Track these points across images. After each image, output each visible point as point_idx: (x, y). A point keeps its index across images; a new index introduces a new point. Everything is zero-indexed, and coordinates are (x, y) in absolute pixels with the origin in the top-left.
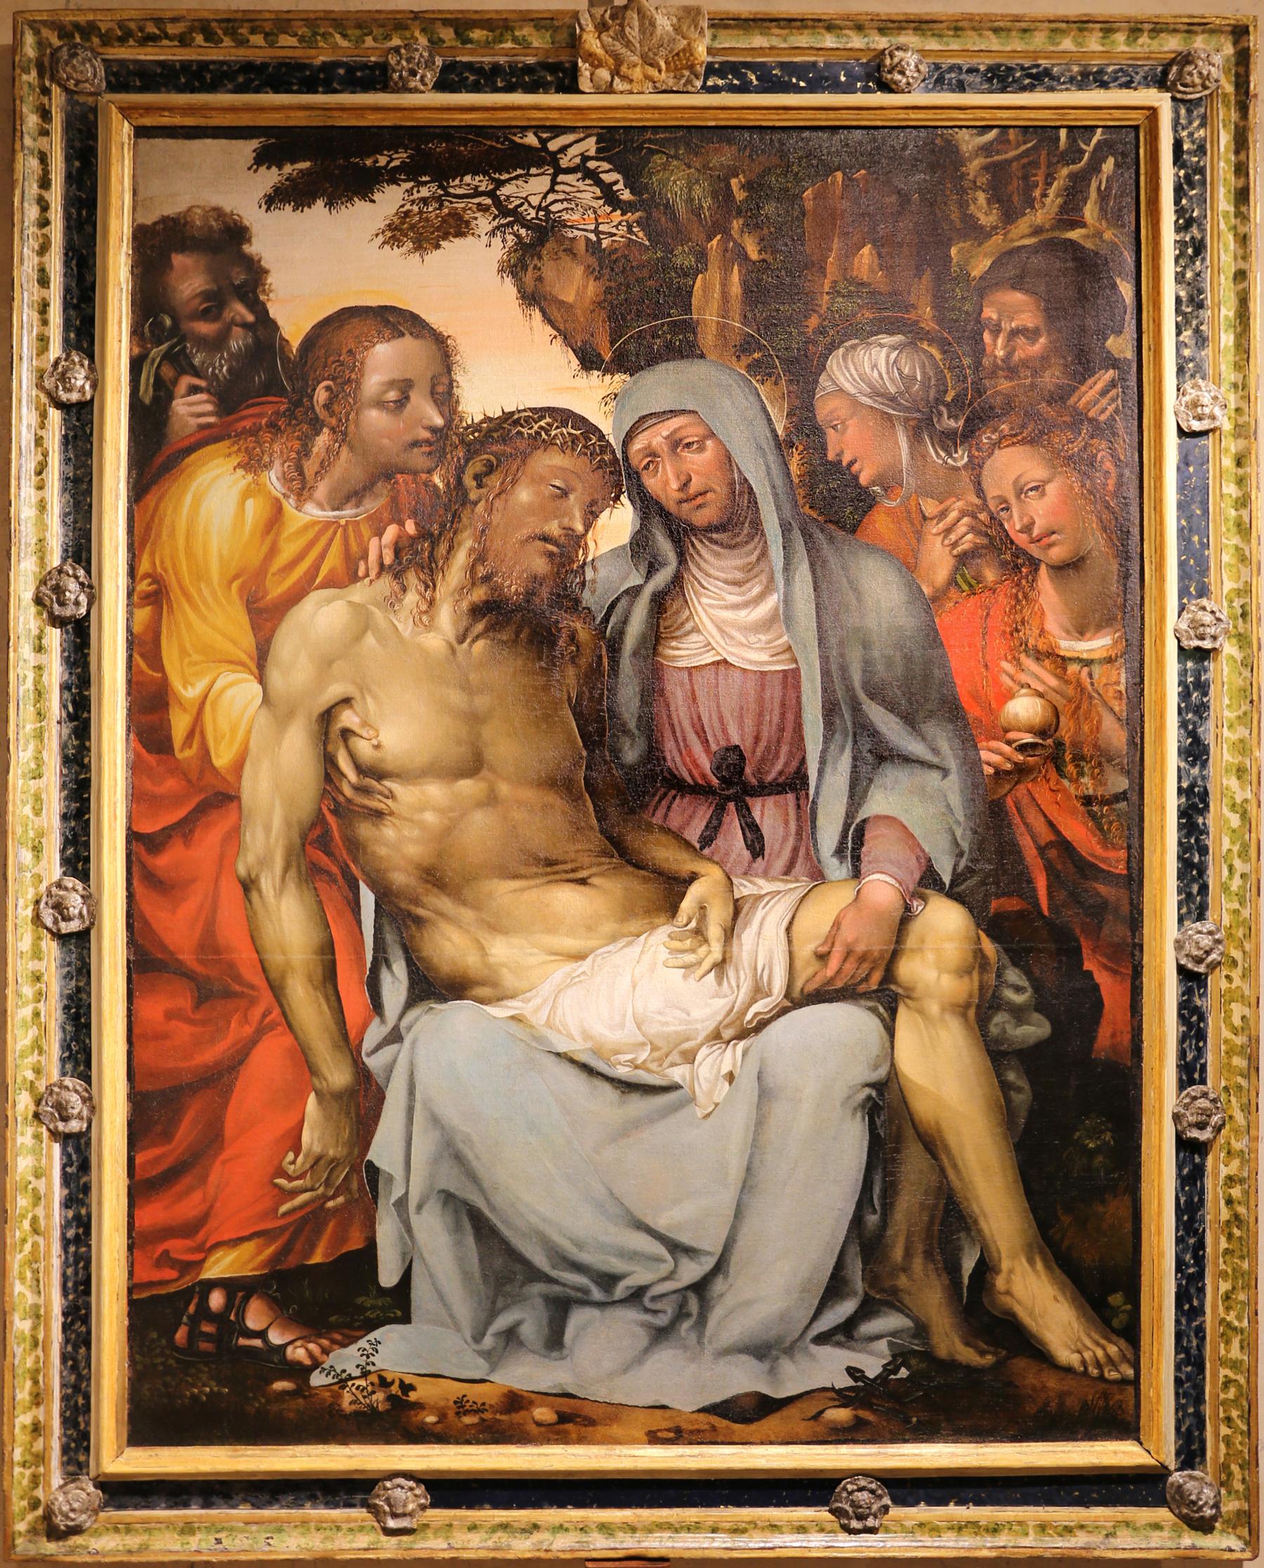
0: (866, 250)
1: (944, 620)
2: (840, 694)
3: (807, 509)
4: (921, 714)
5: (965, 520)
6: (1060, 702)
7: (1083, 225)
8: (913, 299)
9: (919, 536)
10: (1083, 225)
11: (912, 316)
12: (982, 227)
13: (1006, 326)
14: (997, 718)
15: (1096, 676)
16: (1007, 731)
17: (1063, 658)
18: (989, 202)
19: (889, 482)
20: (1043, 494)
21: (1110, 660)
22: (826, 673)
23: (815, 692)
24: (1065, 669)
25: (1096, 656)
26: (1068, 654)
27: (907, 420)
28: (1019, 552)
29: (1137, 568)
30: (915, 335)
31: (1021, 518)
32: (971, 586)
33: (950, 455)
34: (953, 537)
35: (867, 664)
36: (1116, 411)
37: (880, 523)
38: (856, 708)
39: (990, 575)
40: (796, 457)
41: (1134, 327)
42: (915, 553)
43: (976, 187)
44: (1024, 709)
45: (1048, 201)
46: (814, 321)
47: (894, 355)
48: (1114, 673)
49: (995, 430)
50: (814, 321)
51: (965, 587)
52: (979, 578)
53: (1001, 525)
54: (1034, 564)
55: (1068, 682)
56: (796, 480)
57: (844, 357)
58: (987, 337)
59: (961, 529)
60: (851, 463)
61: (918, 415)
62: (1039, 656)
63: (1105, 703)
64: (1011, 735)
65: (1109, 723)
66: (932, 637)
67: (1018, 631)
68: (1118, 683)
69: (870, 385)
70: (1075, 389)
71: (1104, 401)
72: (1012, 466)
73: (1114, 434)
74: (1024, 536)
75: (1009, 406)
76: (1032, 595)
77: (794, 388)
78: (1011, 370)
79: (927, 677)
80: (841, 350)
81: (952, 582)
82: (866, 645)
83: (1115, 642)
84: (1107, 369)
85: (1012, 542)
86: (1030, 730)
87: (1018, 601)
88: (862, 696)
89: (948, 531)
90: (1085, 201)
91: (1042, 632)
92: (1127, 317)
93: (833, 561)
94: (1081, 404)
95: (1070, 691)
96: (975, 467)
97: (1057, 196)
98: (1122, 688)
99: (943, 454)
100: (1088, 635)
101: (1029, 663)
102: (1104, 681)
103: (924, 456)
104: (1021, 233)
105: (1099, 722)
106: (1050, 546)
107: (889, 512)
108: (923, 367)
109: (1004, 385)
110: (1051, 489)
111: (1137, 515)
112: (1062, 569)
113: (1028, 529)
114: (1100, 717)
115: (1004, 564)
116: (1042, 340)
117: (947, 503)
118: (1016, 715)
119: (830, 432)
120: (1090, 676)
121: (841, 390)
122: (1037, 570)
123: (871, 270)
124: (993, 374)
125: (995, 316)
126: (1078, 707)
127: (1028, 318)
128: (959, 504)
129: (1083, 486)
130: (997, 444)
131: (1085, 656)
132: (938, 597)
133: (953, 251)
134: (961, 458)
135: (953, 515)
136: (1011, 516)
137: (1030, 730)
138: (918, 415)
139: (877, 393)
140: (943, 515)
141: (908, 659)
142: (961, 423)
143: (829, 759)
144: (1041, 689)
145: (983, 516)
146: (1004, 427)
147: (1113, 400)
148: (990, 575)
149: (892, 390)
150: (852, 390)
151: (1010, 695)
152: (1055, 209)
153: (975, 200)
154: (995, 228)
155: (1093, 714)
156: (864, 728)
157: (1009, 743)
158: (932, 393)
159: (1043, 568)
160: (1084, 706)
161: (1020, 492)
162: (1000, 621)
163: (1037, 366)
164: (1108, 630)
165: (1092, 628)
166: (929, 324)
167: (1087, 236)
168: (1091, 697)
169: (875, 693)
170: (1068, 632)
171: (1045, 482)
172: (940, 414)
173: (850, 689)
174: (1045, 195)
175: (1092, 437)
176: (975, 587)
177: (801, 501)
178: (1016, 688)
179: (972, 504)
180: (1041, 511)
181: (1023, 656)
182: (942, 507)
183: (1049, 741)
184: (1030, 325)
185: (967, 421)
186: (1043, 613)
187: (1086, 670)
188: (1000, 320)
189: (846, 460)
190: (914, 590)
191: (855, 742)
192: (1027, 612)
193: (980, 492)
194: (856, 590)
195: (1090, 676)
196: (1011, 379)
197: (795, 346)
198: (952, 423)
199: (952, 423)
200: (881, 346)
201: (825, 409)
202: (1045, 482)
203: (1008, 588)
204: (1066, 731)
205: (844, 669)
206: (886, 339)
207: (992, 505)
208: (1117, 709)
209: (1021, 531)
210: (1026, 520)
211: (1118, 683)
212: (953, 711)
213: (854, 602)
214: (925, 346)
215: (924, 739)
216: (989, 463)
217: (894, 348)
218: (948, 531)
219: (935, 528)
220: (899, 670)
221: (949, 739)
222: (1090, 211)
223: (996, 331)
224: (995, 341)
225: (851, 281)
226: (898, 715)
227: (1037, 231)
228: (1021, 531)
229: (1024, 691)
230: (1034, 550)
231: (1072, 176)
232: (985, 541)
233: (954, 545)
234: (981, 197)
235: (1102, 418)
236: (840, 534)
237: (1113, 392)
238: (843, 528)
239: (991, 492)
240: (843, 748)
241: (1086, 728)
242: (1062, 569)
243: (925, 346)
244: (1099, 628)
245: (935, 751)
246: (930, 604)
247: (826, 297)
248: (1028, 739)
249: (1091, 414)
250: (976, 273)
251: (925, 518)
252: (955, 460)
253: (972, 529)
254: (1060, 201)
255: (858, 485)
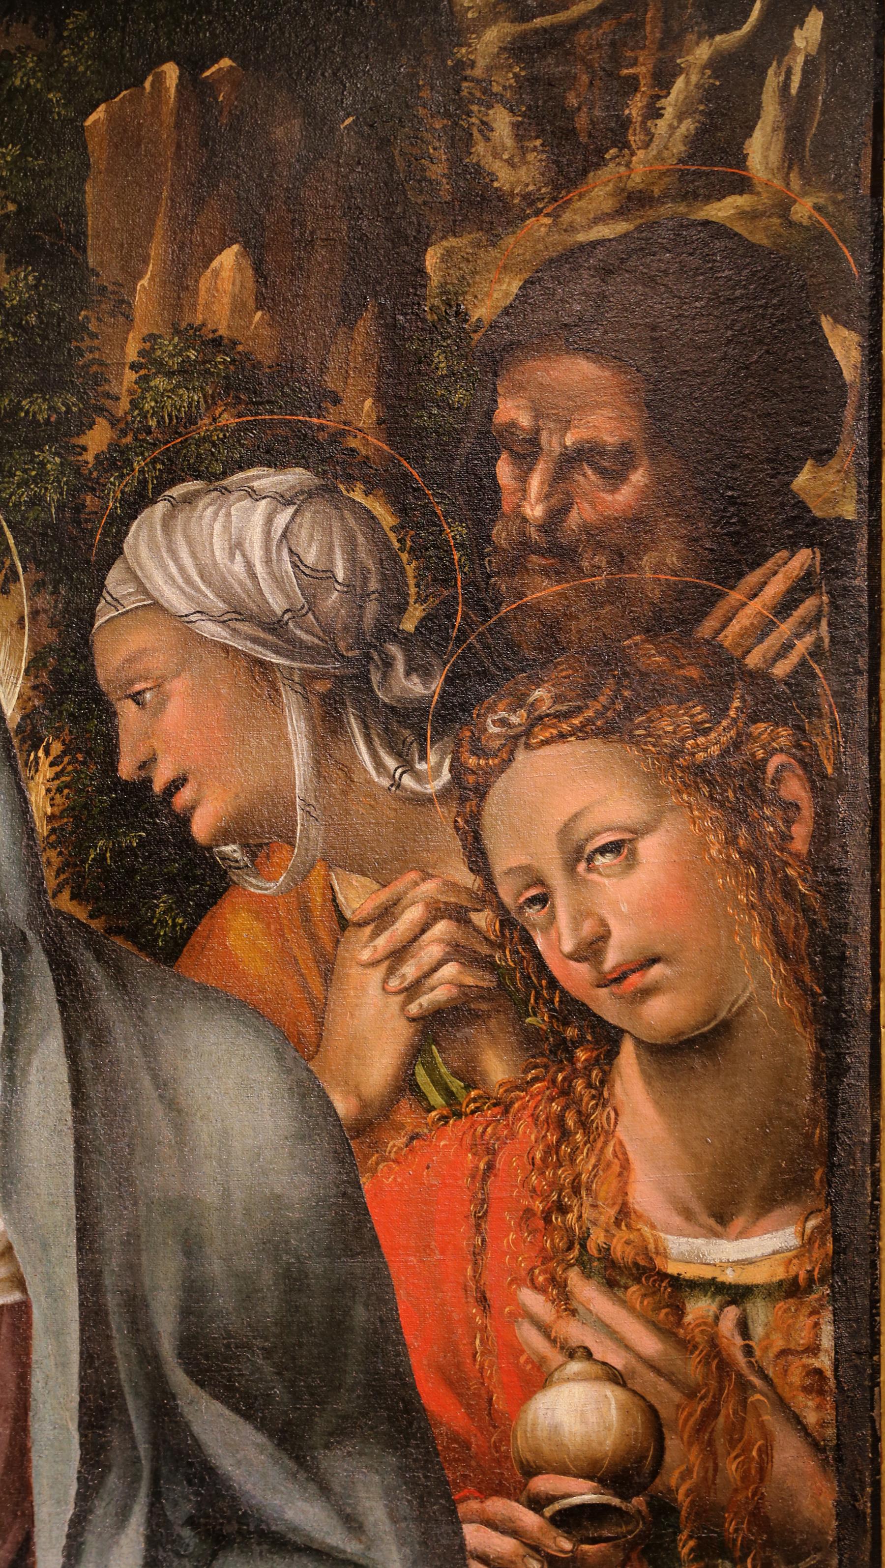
0: (228, 259)
1: (385, 1183)
2: (125, 1369)
3: (65, 903)
4: (321, 1424)
5: (441, 928)
6: (666, 1397)
7: (743, 185)
8: (330, 382)
9: (328, 969)
10: (743, 185)
11: (331, 421)
12: (500, 196)
13: (552, 443)
14: (506, 1437)
15: (758, 1330)
16: (530, 1471)
17: (677, 1283)
18: (520, 133)
19: (261, 832)
20: (632, 862)
21: (791, 1289)
22: (92, 1315)
23: (63, 1365)
24: (679, 1311)
25: (758, 1276)
26: (690, 1272)
27: (310, 677)
28: (573, 1009)
29: (865, 1051)
30: (333, 466)
31: (576, 924)
32: (448, 1094)
33: (407, 766)
34: (410, 971)
35: (194, 1296)
36: (816, 652)
37: (239, 935)
38: (163, 1410)
39: (498, 1068)
40: (46, 771)
41: (862, 441)
42: (320, 1013)
43: (490, 99)
44: (575, 1413)
45: (661, 126)
46: (97, 439)
47: (283, 518)
48: (805, 1322)
49: (519, 701)
50: (97, 439)
51: (436, 1098)
52: (470, 1077)
53: (528, 941)
54: (608, 1039)
55: (685, 1345)
56: (42, 828)
57: (167, 522)
58: (504, 471)
59: (431, 949)
60: (176, 785)
61: (333, 666)
62: (613, 1274)
63: (782, 1404)
64: (543, 1484)
65: (790, 1457)
66: (350, 1223)
67: (563, 1210)
68: (814, 1349)
69: (223, 591)
70: (712, 599)
71: (786, 628)
72: (562, 789)
73: (814, 711)
74: (583, 970)
75: (552, 637)
76: (599, 1118)
77: (44, 600)
78: (558, 550)
79: (338, 1325)
80: (160, 508)
81: (405, 1085)
82: (191, 1247)
83: (808, 1243)
84: (793, 546)
85: (553, 983)
86: (591, 1470)
87: (565, 1134)
88: (178, 1378)
89: (398, 955)
90: (749, 131)
91: (624, 1214)
92: (849, 413)
93: (109, 1005)
94: (729, 636)
95: (692, 1369)
96: (469, 794)
97: (680, 117)
98: (824, 1362)
99: (391, 763)
100: (740, 1222)
101: (588, 1293)
102: (779, 1343)
103: (348, 769)
104: (593, 218)
105: (766, 1452)
106: (647, 992)
107: (262, 908)
108: (351, 542)
109: (544, 591)
110: (650, 848)
111: (865, 912)
112: (672, 1055)
113: (591, 950)
114: (767, 1436)
115: (530, 1040)
116: (638, 477)
117: (399, 885)
118: (556, 1429)
119: (127, 711)
120: (743, 1327)
121: (156, 606)
122: (612, 1054)
123: (238, 308)
124: (515, 565)
125: (525, 420)
126: (711, 1414)
127: (605, 424)
128: (429, 887)
129: (731, 841)
130: (519, 739)
131: (730, 1276)
132: (370, 1124)
133: (432, 259)
134: (435, 772)
135: (412, 915)
136: (552, 918)
137: (591, 1470)
138: (333, 666)
139: (237, 613)
140: (385, 916)
141: (293, 1281)
142: (437, 685)
143: (91, 1541)
144: (618, 1360)
145: (482, 919)
146: (542, 695)
147: (811, 624)
148: (498, 1068)
149: (277, 603)
150: (179, 604)
151: (539, 1378)
152: (678, 148)
153: (486, 127)
154: (529, 199)
155: (751, 1430)
156: (180, 1460)
157: (536, 1504)
158: (372, 608)
159: (628, 1048)
160: (728, 1409)
161: (577, 856)
162: (518, 1180)
163: (623, 541)
164: (791, 1210)
165: (749, 1204)
166: (368, 442)
167: (750, 216)
168: (744, 1386)
169: (211, 1363)
170: (687, 1214)
171: (638, 832)
172: (388, 664)
173: (149, 1358)
174: (654, 112)
175: (754, 719)
176: (463, 1100)
177: (51, 882)
178: (555, 1357)
179: (454, 887)
180: (629, 902)
181: (574, 1277)
182: (384, 896)
183: (638, 1502)
184: (611, 439)
185: (449, 681)
186: (626, 1165)
187: (732, 1313)
188: (538, 431)
189: (160, 779)
190: (310, 1096)
191: (156, 1495)
192: (586, 1164)
193: (478, 857)
194: (172, 1106)
195: (743, 1327)
196: (559, 575)
197: (52, 496)
198: (416, 687)
199: (416, 687)
200: (254, 495)
201: (120, 650)
202: (638, 832)
203: (539, 1101)
204: (680, 1468)
205: (136, 1305)
206: (267, 479)
207: (506, 892)
208: (811, 1418)
209: (576, 956)
210: (588, 928)
211: (814, 1349)
212: (395, 1417)
213: (167, 1133)
214: (358, 496)
215: (325, 1490)
216: (500, 785)
217: (283, 500)
218: (398, 955)
219: (367, 948)
220: (269, 1307)
221: (388, 1493)
222: (761, 150)
223: (527, 453)
224: (523, 480)
225: (192, 335)
226: (262, 1426)
227: (632, 201)
228: (576, 956)
229: (575, 1367)
230: (606, 1005)
231: (720, 64)
232: (487, 981)
233: (412, 990)
234: (502, 122)
235: (781, 669)
236: (140, 963)
237: (809, 605)
238: (148, 948)
239: (505, 857)
240: (123, 1515)
241: (731, 1468)
242: (672, 1055)
243: (358, 496)
244: (767, 1203)
245: (352, 1523)
246: (347, 1142)
247: (130, 376)
248: (584, 1493)
249: (753, 660)
250: (482, 311)
251: (343, 923)
252: (418, 777)
253: (457, 951)
254: (688, 126)
255: (186, 841)
